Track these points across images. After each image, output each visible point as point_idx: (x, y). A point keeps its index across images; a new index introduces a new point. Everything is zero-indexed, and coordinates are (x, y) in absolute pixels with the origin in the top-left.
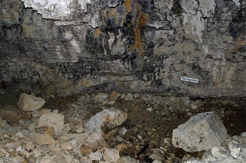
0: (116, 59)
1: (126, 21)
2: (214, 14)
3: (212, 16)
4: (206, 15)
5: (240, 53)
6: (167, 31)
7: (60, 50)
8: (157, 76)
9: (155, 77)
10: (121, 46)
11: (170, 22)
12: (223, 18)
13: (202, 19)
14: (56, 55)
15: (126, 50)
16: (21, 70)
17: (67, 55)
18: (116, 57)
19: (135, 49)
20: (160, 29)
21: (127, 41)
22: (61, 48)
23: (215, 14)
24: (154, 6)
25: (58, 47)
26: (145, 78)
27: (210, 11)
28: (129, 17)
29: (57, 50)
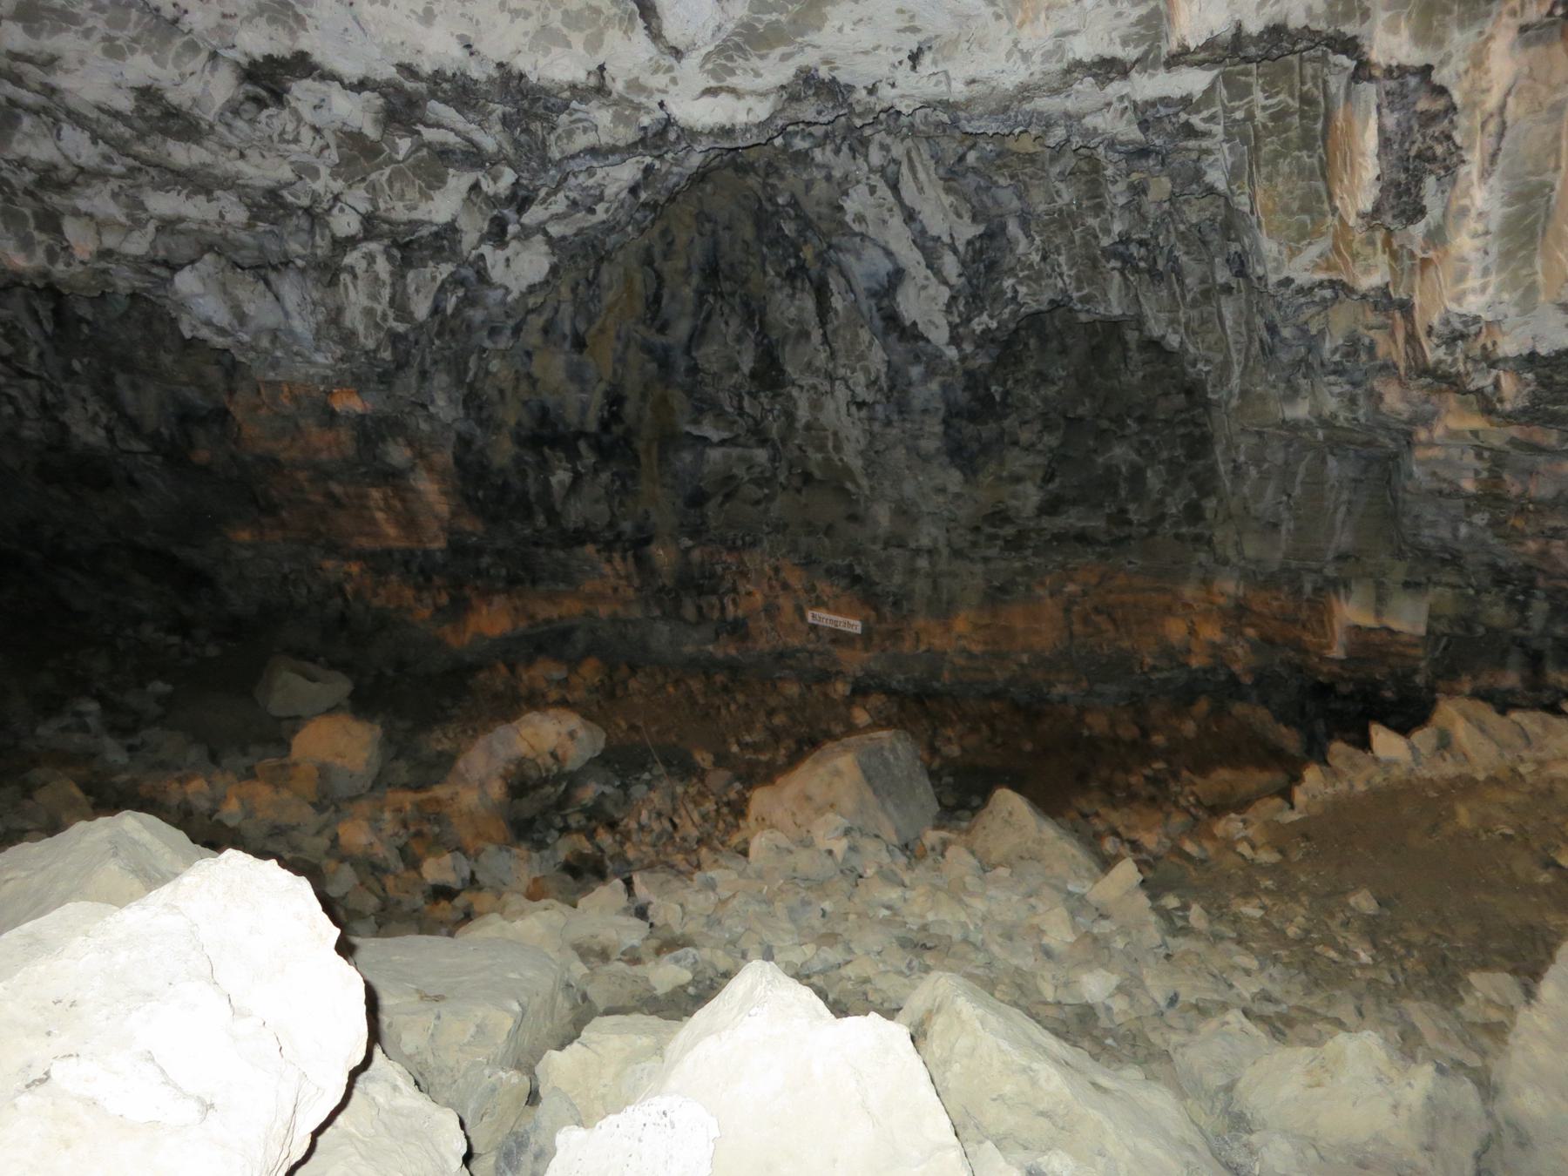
0: (582, 543)
1: (606, 414)
2: (885, 388)
3: (879, 396)
4: (863, 394)
5: (993, 530)
6: (747, 452)
7: (382, 504)
8: (730, 608)
9: (723, 609)
10: (597, 501)
11: (757, 423)
12: (917, 403)
13: (853, 409)
14: (373, 521)
15: (613, 514)
16: (285, 577)
17: (409, 523)
18: (579, 537)
19: (646, 512)
20: (723, 443)
21: (613, 481)
22: (385, 499)
23: (892, 388)
24: (696, 364)
25: (376, 494)
26: (689, 612)
27: (874, 383)
28: (615, 399)
29: (371, 503)
